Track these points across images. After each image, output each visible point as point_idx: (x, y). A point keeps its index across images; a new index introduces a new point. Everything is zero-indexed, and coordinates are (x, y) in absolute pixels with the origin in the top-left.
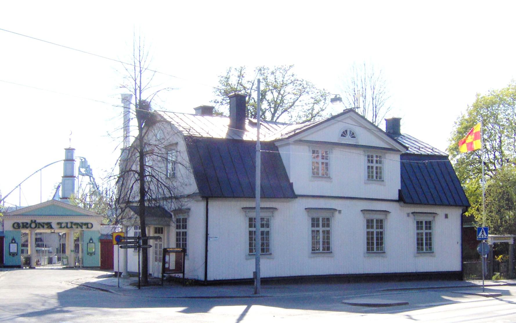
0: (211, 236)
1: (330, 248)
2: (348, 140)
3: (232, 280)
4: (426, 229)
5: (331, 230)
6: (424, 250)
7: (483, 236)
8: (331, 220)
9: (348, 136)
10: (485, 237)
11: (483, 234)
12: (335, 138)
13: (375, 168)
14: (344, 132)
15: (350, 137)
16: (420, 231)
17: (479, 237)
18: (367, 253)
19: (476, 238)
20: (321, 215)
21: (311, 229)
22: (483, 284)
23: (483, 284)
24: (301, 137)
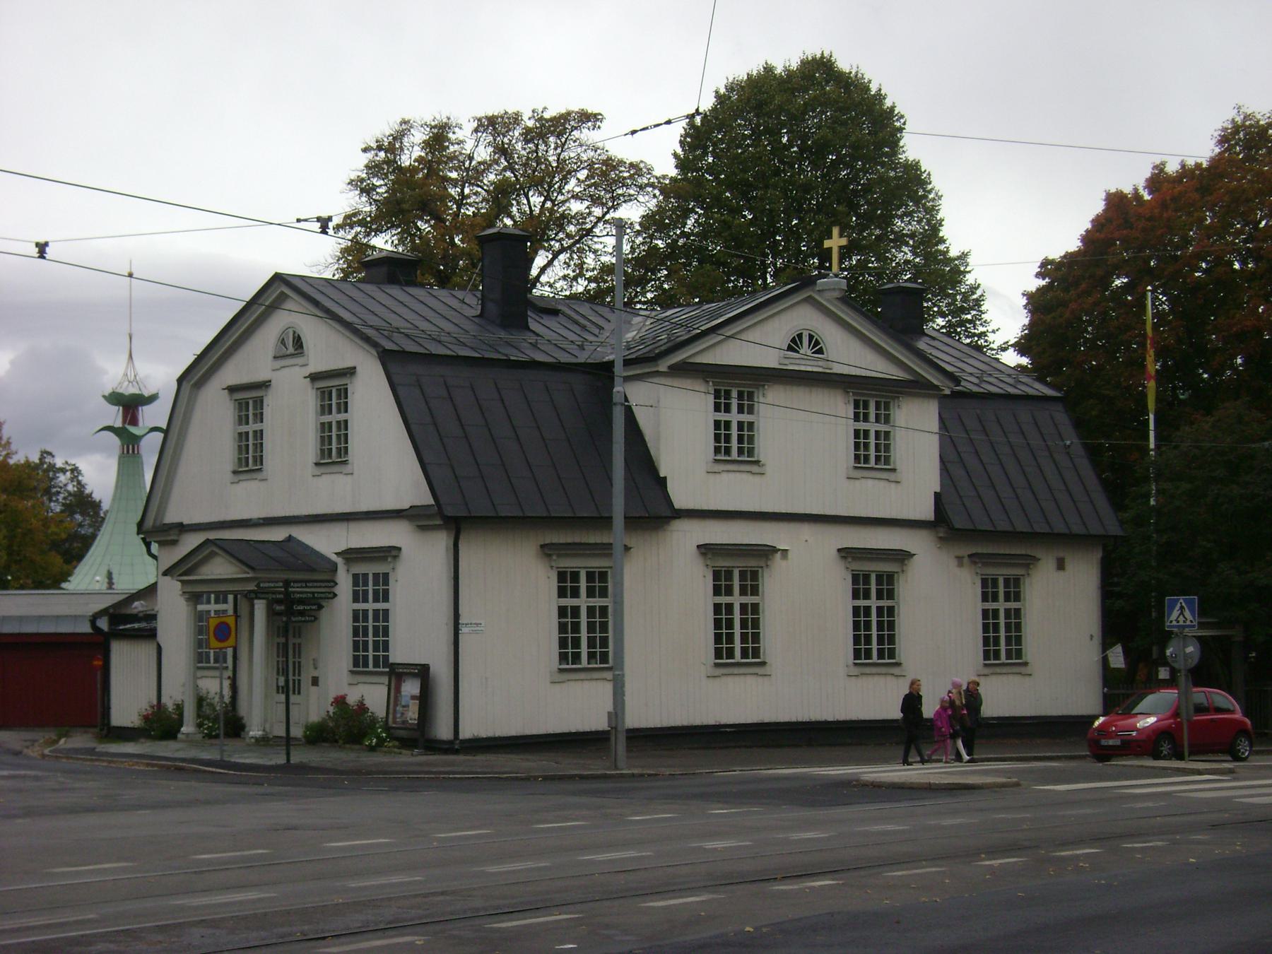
0: (464, 622)
1: (762, 651)
2: (805, 362)
3: (683, 728)
4: (743, 592)
5: (764, 603)
6: (875, 659)
7: (1181, 618)
8: (763, 577)
9: (805, 349)
10: (1188, 623)
11: (1182, 613)
12: (769, 359)
13: (734, 427)
14: (793, 340)
15: (809, 353)
16: (569, 602)
17: (1171, 622)
18: (855, 664)
19: (1163, 622)
20: (736, 565)
21: (980, 606)
22: (288, 760)
23: (288, 760)
24: (684, 356)
